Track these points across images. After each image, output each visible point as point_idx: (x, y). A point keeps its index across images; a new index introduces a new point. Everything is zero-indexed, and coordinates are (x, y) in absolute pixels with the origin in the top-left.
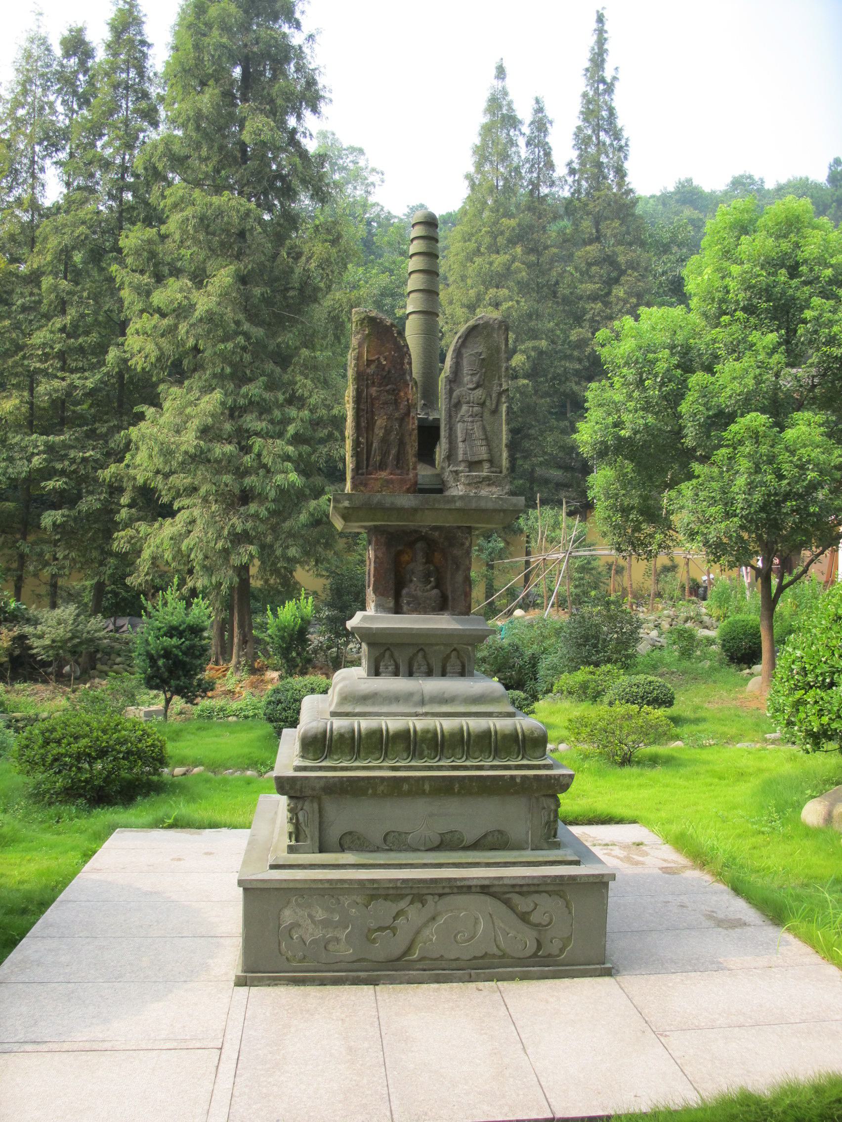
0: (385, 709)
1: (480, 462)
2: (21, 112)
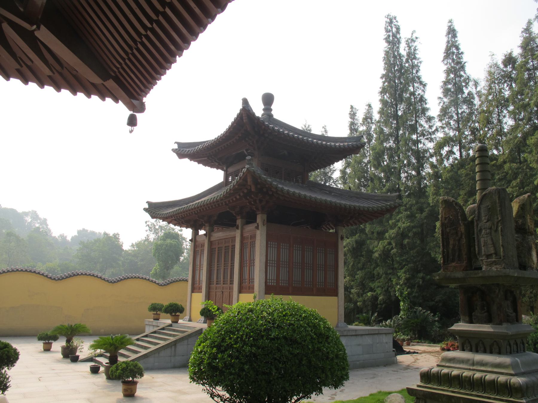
0: (458, 366)
1: (491, 255)
2: (490, 97)
